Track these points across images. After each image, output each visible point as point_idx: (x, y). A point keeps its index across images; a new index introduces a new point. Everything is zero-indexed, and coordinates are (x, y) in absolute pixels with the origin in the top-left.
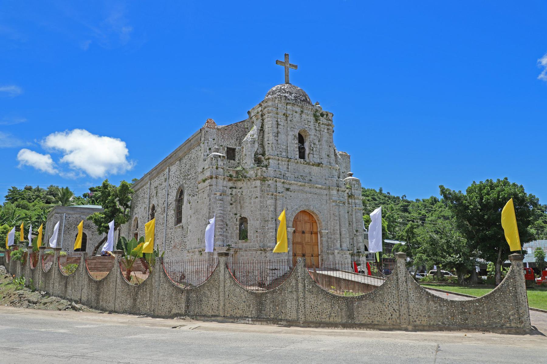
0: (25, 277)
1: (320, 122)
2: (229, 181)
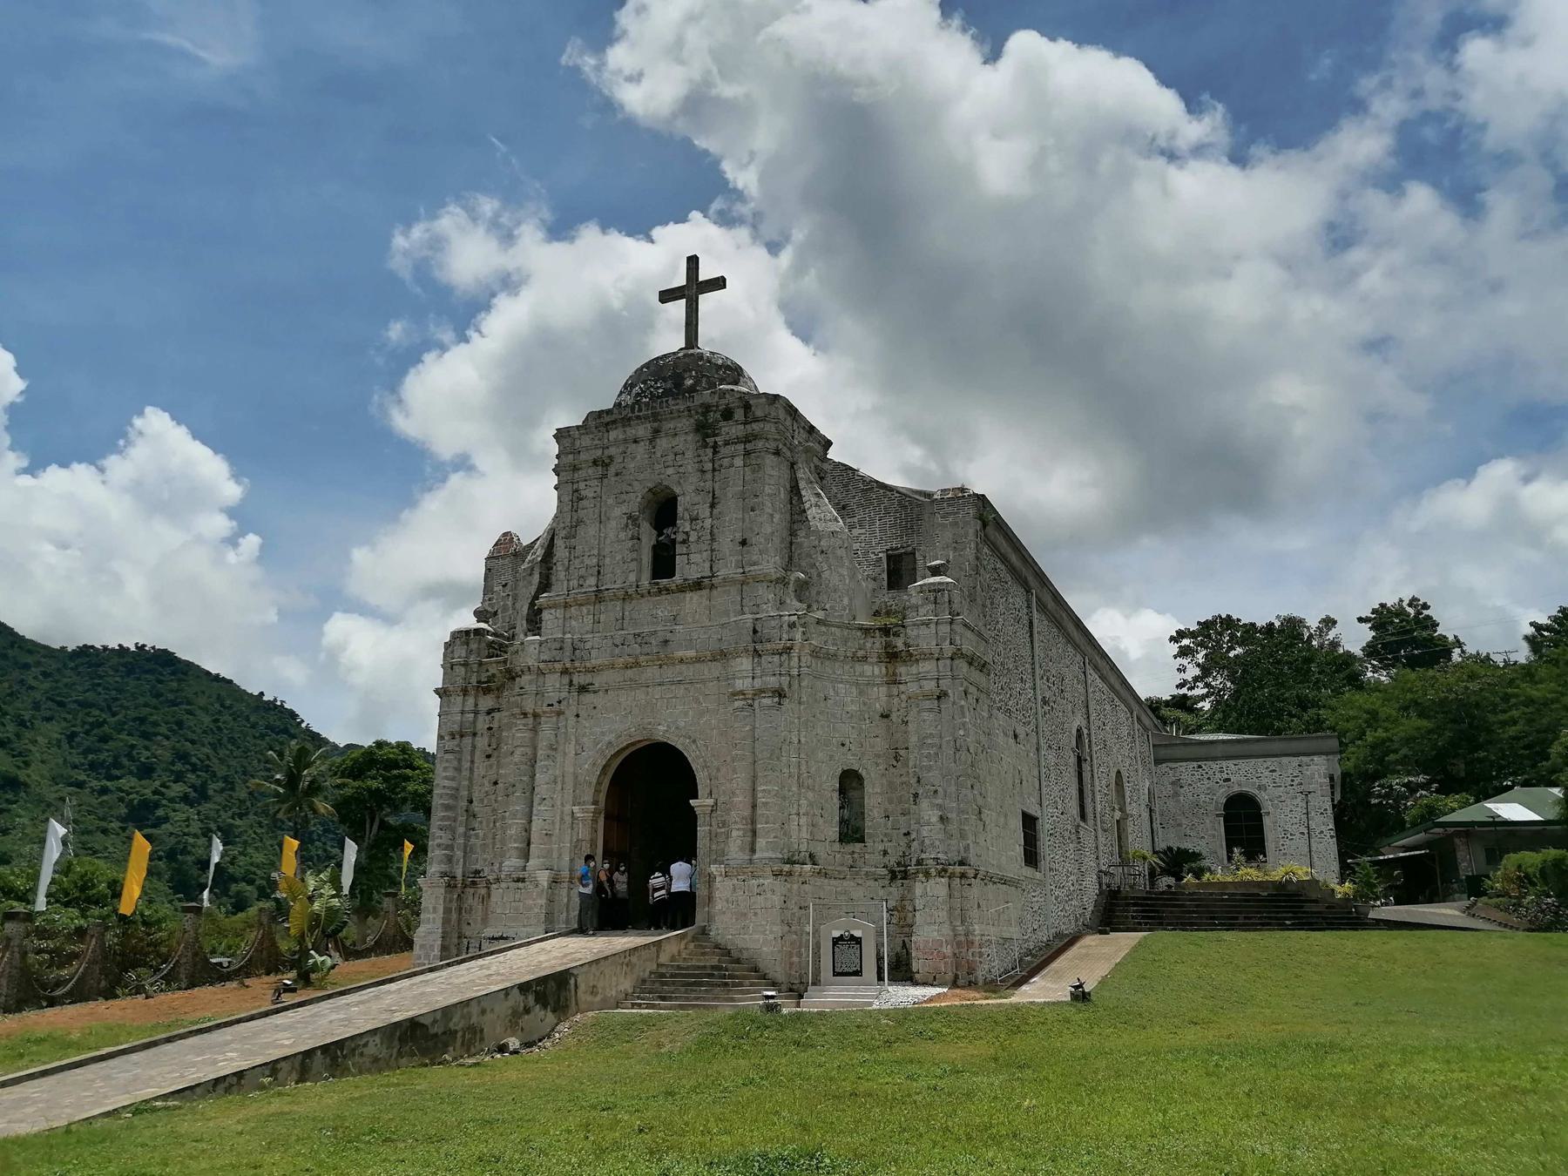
0: (213, 952)
1: (716, 442)
2: (875, 615)
